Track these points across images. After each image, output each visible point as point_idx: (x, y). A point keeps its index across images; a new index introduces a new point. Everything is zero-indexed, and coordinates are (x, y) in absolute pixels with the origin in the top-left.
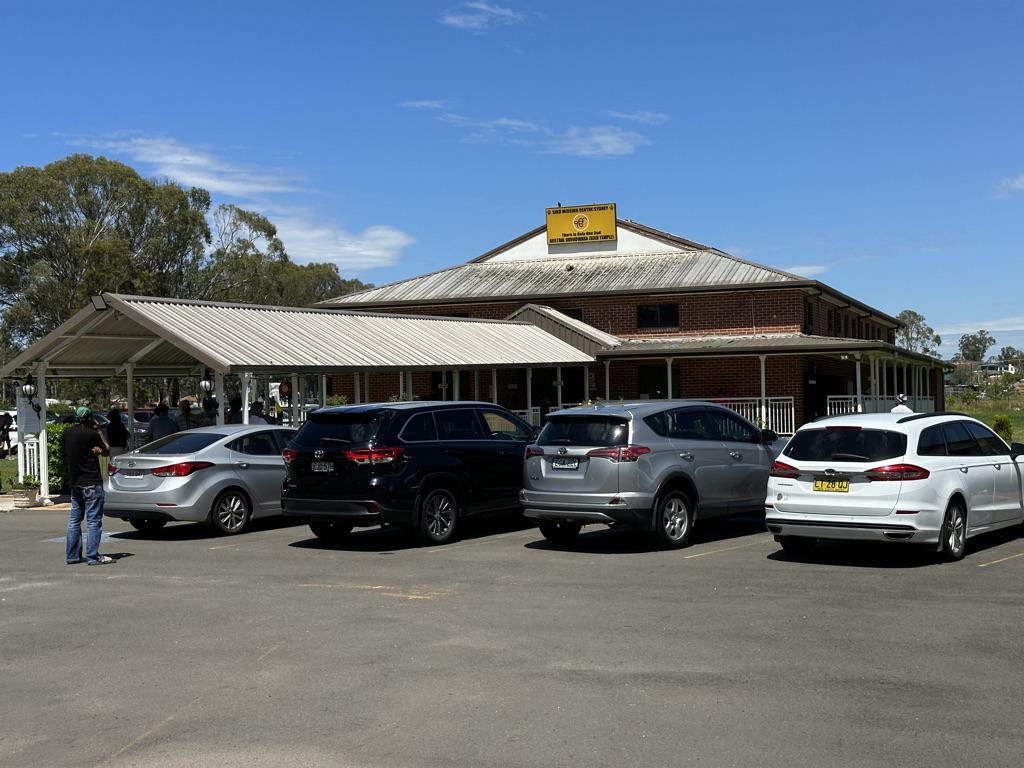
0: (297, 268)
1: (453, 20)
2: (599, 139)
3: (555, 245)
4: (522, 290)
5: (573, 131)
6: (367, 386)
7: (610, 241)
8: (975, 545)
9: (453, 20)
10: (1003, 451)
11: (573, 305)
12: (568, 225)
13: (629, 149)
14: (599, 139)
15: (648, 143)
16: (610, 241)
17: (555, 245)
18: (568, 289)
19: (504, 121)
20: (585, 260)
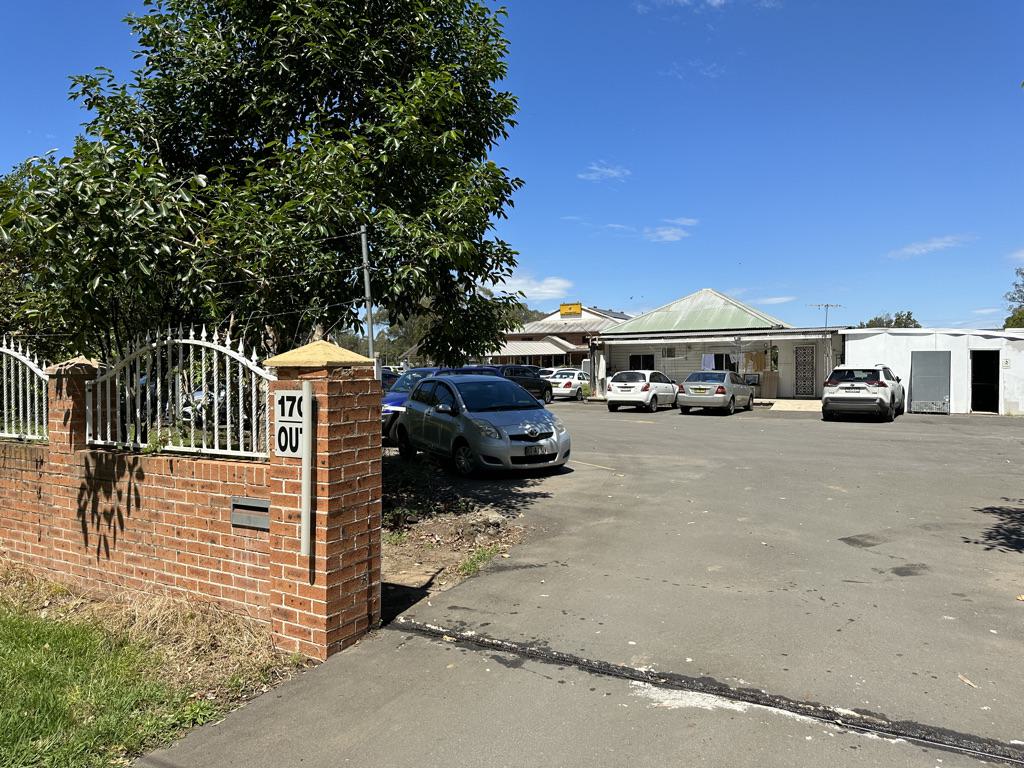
0: (551, 276)
1: (581, 176)
2: (662, 233)
3: (563, 316)
4: (549, 331)
5: (646, 230)
6: (5, 392)
7: (579, 315)
8: (660, 409)
9: (581, 176)
10: (669, 382)
11: (562, 336)
12: (566, 310)
13: (677, 239)
14: (662, 233)
15: (687, 235)
16: (579, 315)
17: (563, 316)
18: (562, 331)
19: (611, 225)
20: (570, 321)
